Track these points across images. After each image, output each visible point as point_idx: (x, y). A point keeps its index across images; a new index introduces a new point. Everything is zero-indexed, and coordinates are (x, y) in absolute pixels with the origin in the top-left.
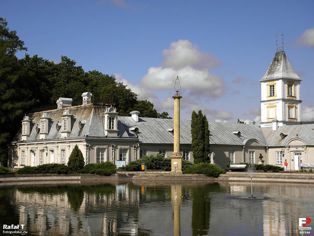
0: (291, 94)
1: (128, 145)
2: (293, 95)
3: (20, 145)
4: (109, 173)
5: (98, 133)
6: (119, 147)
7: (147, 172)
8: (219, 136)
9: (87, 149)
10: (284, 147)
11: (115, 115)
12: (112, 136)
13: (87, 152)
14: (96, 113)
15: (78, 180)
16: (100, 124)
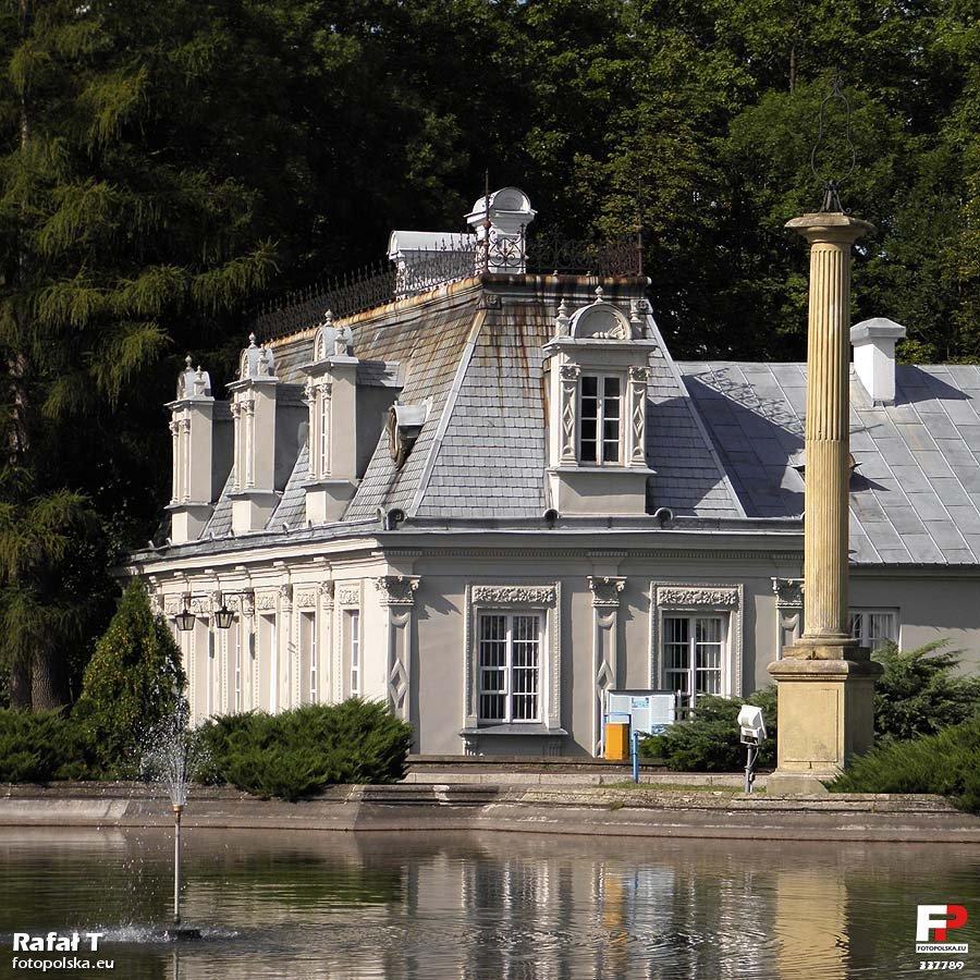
1: (728, 581)
4: (301, 782)
5: (496, 492)
6: (658, 593)
7: (643, 778)
9: (396, 610)
11: (622, 360)
12: (596, 515)
13: (394, 629)
14: (498, 347)
15: (107, 826)
16: (518, 427)
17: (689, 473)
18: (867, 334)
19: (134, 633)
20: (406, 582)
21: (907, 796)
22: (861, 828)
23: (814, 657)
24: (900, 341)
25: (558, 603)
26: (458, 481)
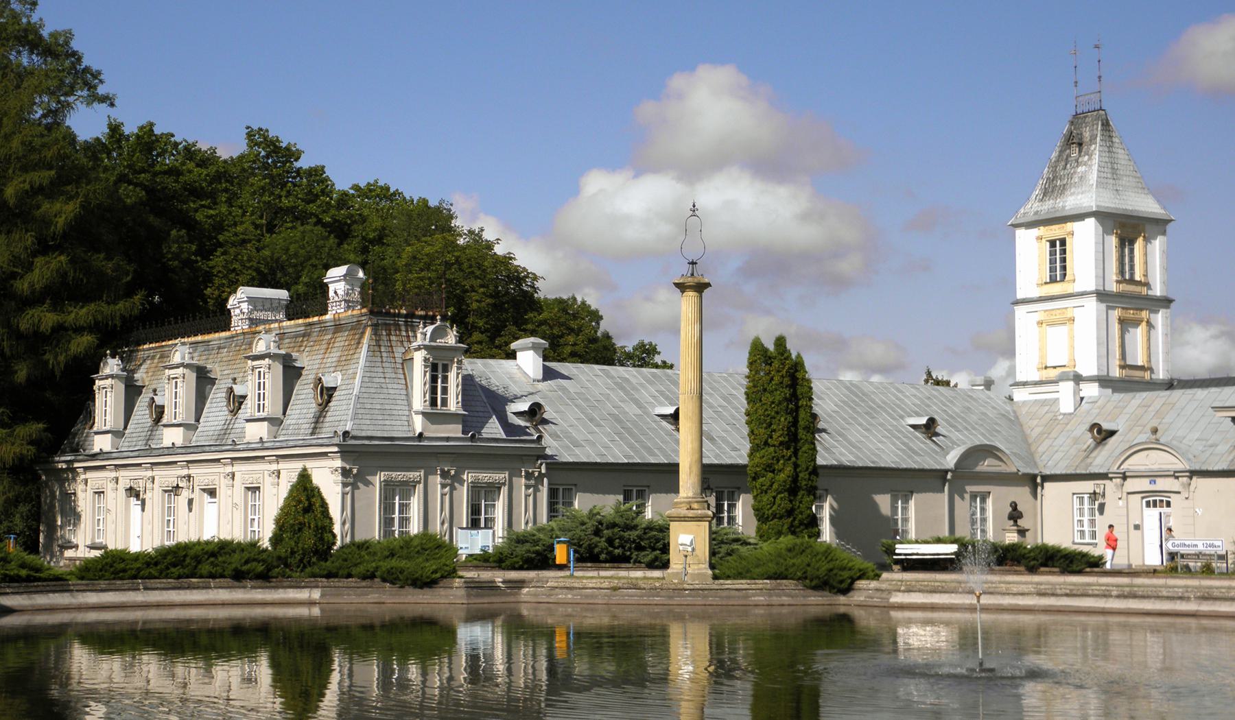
0: (1132, 274)
1: (501, 469)
2: (1137, 278)
3: (86, 469)
4: (428, 577)
5: (387, 422)
6: (468, 477)
8: (855, 434)
9: (345, 485)
10: (1104, 476)
12: (443, 435)
13: (344, 494)
14: (380, 346)
15: (311, 603)
16: (395, 388)
17: (476, 414)
18: (531, 345)
19: (307, 496)
20: (351, 470)
21: (778, 581)
22: (762, 598)
23: (691, 508)
24: (545, 349)
25: (422, 481)
26: (368, 417)
